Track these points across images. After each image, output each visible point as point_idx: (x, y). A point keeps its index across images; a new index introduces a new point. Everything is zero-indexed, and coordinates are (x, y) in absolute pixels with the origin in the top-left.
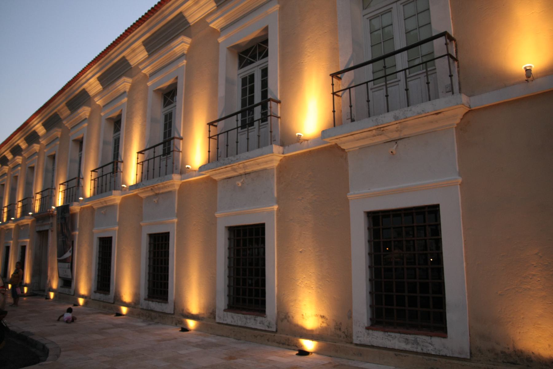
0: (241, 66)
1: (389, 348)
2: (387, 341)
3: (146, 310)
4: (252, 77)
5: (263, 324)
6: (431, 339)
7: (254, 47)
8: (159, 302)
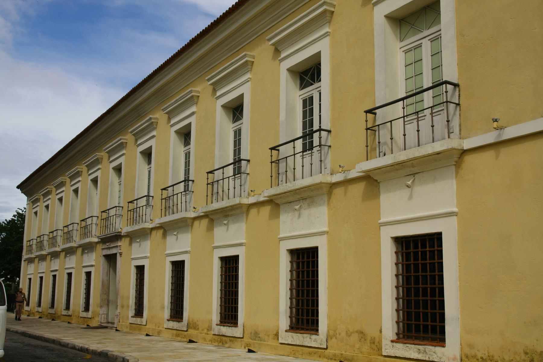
0: (318, 81)
1: (407, 358)
2: (406, 352)
3: (218, 335)
4: (311, 99)
5: (317, 342)
6: (435, 348)
7: (314, 67)
8: (229, 326)
